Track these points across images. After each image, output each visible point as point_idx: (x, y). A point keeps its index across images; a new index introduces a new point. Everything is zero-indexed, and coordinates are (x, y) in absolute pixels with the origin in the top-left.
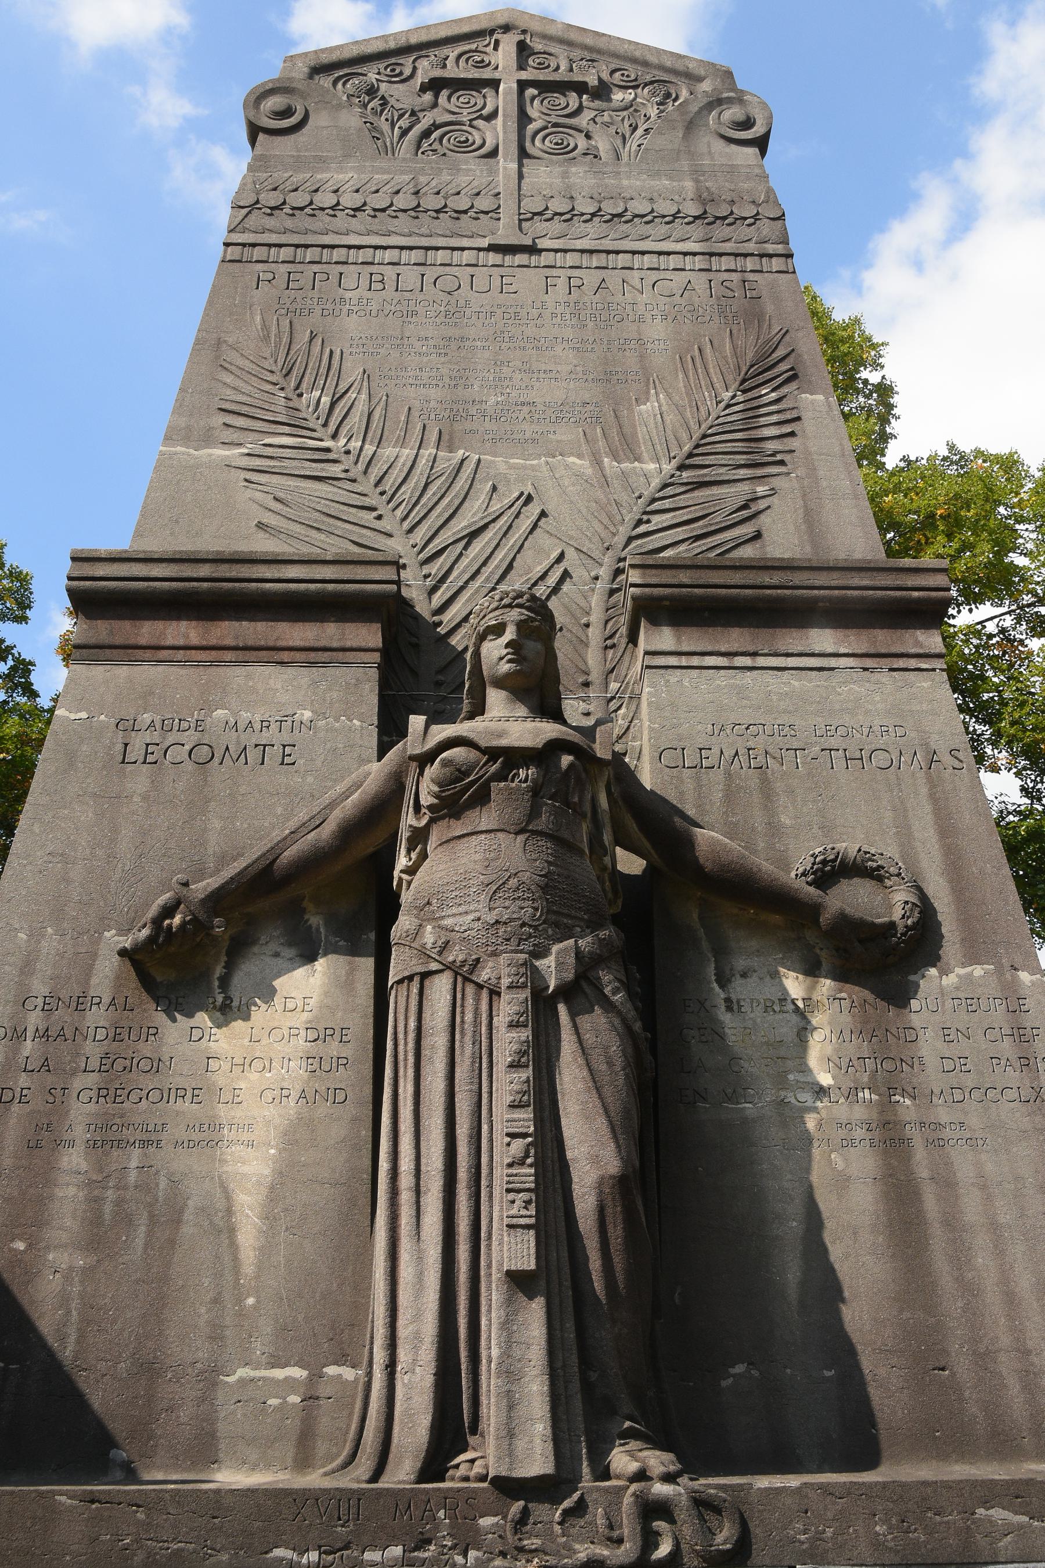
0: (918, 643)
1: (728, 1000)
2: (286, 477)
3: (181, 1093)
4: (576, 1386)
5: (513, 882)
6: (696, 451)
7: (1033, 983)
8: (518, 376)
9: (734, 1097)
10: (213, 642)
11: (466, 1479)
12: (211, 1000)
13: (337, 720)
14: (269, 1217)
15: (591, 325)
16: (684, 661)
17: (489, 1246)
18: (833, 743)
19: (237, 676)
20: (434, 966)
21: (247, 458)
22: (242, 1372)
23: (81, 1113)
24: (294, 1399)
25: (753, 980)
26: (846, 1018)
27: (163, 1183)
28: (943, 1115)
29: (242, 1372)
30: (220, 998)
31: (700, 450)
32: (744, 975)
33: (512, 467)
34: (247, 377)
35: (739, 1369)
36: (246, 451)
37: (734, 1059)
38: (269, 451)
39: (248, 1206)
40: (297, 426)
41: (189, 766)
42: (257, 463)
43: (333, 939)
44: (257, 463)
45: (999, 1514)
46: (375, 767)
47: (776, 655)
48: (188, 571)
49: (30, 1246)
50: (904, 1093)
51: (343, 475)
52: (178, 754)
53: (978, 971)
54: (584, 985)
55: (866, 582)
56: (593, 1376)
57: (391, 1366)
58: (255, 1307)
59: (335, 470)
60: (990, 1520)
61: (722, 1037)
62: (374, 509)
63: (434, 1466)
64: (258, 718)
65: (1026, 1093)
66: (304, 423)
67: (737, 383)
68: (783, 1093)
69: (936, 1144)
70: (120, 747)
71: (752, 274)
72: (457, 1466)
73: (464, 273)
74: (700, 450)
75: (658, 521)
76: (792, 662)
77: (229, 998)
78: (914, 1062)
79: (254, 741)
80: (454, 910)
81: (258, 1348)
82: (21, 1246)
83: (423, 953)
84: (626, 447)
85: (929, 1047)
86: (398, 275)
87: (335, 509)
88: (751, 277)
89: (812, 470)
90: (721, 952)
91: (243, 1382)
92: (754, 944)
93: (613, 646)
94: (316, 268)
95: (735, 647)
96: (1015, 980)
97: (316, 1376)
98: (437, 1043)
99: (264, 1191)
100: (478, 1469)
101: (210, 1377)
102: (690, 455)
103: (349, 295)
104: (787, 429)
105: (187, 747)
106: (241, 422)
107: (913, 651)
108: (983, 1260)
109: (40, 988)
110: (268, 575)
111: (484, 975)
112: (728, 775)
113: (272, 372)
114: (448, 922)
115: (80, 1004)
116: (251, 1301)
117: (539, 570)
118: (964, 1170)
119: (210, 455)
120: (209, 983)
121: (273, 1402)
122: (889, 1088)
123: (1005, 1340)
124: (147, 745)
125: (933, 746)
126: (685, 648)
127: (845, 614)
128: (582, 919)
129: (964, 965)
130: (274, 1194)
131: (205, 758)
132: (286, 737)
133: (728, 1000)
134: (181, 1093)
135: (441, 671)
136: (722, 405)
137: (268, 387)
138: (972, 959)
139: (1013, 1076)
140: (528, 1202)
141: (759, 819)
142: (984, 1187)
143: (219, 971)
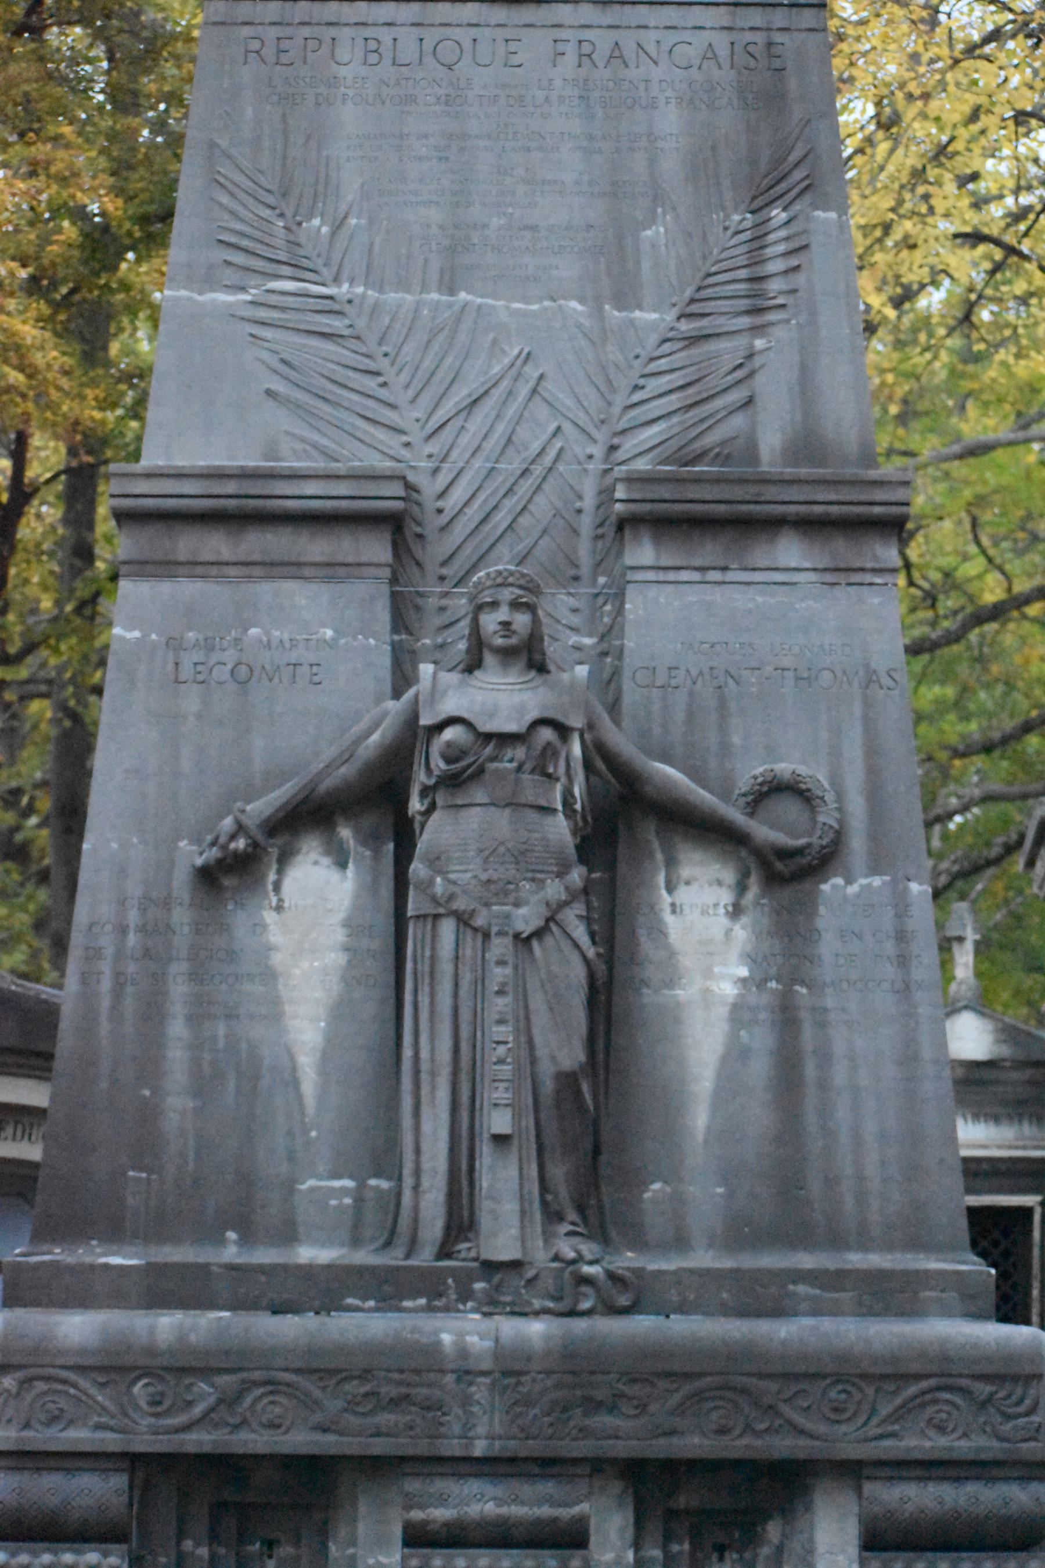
0: (875, 558)
1: (673, 905)
2: (290, 332)
3: (250, 976)
4: (537, 1205)
5: (502, 849)
6: (698, 296)
7: (920, 892)
8: (521, 190)
9: (670, 983)
10: (242, 557)
11: (464, 1260)
12: (267, 902)
13: (355, 639)
14: (323, 1072)
15: (600, 114)
16: (661, 576)
17: (481, 1115)
18: (786, 662)
19: (265, 590)
20: (441, 911)
21: (250, 306)
22: (311, 1183)
23: (179, 990)
24: (348, 1201)
25: (694, 887)
26: (765, 921)
27: (244, 1046)
28: (830, 1002)
29: (311, 1183)
30: (274, 900)
31: (704, 294)
32: (688, 883)
33: (516, 313)
34: (243, 197)
35: (656, 1186)
36: (249, 298)
37: (672, 954)
38: (273, 299)
39: (307, 1065)
40: (298, 268)
41: (232, 687)
42: (263, 314)
43: (361, 849)
44: (263, 314)
45: (802, 1289)
46: (391, 705)
47: (746, 569)
48: (217, 488)
49: (153, 1093)
50: (803, 983)
51: (346, 332)
52: (222, 673)
53: (877, 881)
54: (552, 925)
55: (833, 497)
56: (549, 1198)
57: (416, 1187)
58: (318, 1138)
59: (337, 324)
60: (795, 1294)
61: (665, 935)
62: (378, 374)
63: (445, 1252)
64: (286, 637)
65: (899, 985)
66: (305, 263)
67: (747, 201)
68: (708, 983)
69: (822, 1025)
70: (170, 667)
71: (778, 34)
72: (459, 1251)
73: (464, 36)
74: (704, 294)
75: (654, 385)
76: (758, 576)
77: (280, 900)
78: (812, 959)
79: (285, 661)
80: (458, 868)
81: (321, 1168)
82: (147, 1093)
83: (435, 900)
84: (625, 296)
85: (828, 946)
86: (395, 40)
87: (341, 374)
88: (778, 37)
89: (813, 314)
90: (671, 862)
91: (312, 1189)
92: (697, 856)
93: (602, 536)
94: (307, 31)
95: (707, 562)
96: (906, 889)
97: (362, 1185)
98: (446, 968)
99: (318, 1054)
100: (473, 1254)
101: (289, 1185)
102: (693, 301)
103: (343, 71)
104: (794, 262)
105: (229, 667)
106: (240, 258)
107: (869, 565)
108: (842, 1113)
109: (134, 889)
110: (289, 492)
111: (479, 921)
112: (691, 694)
113: (269, 191)
114: (452, 876)
115: (167, 903)
116: (313, 1134)
117: (536, 446)
118: (839, 1047)
119: (214, 301)
120: (264, 886)
121: (333, 1202)
122: (791, 978)
123: (849, 1171)
124: (196, 664)
125: (873, 665)
126: (665, 562)
127: (812, 526)
128: (552, 872)
129: (866, 876)
130: (325, 1058)
131: (243, 678)
132: (312, 658)
133: (673, 905)
134: (250, 976)
135: (444, 564)
136: (729, 232)
137: (266, 213)
138: (874, 869)
139: (891, 971)
140: (507, 1089)
141: (712, 740)
142: (852, 1059)
143: (272, 877)
